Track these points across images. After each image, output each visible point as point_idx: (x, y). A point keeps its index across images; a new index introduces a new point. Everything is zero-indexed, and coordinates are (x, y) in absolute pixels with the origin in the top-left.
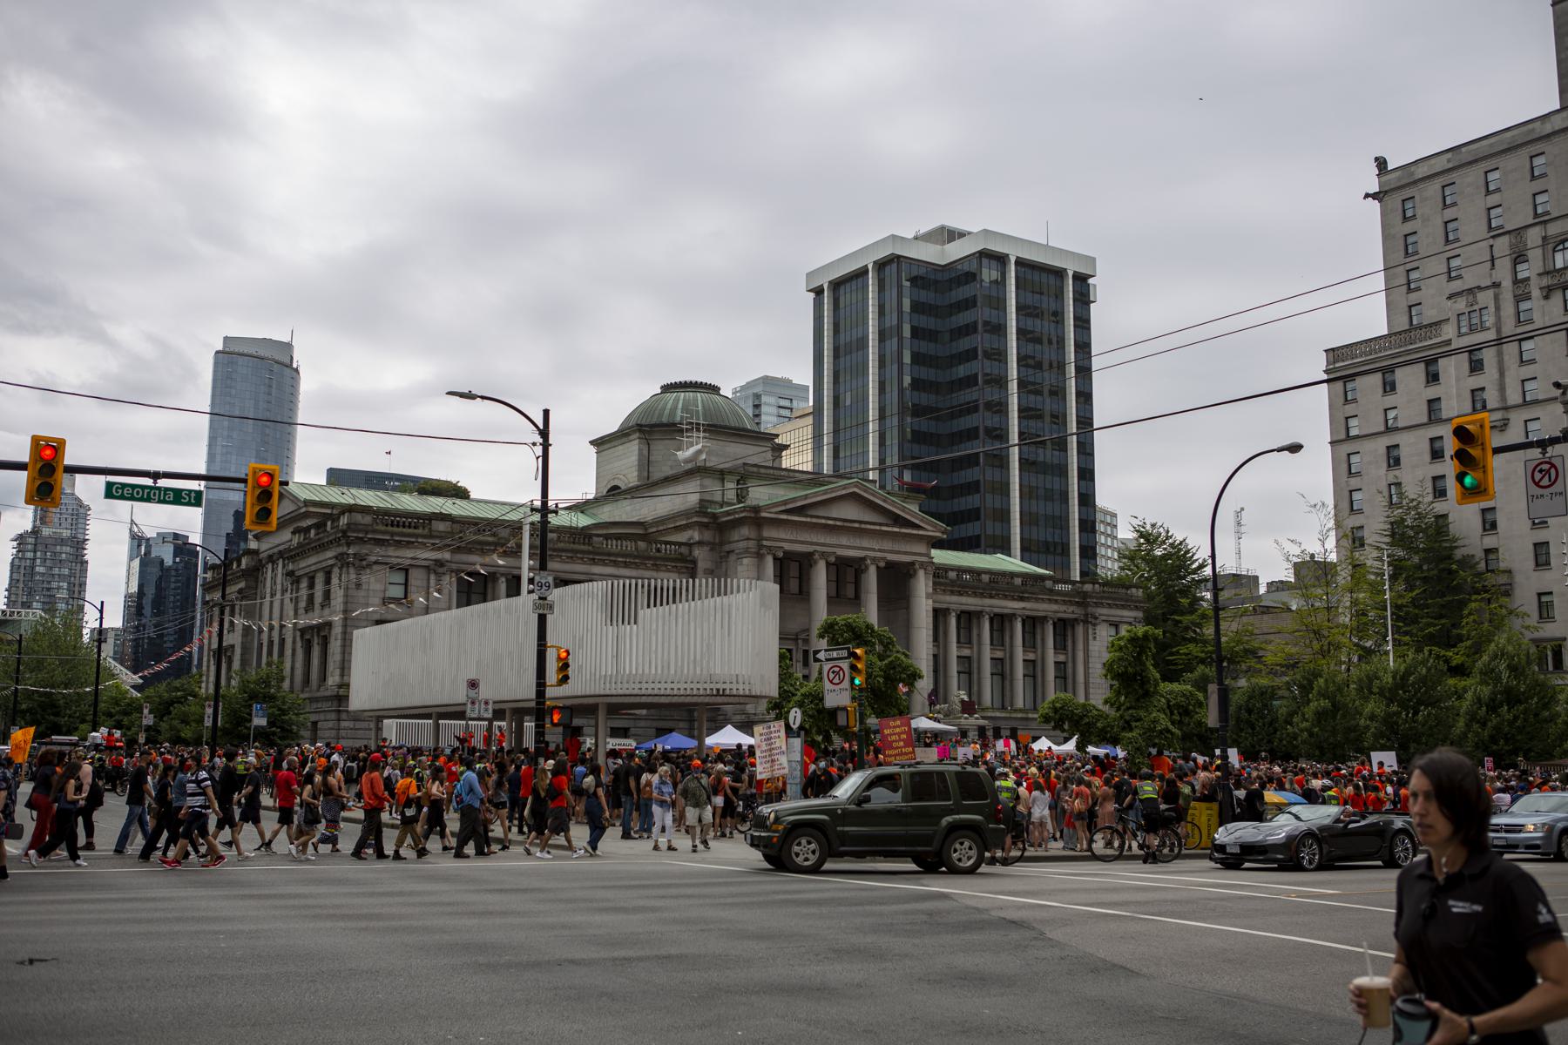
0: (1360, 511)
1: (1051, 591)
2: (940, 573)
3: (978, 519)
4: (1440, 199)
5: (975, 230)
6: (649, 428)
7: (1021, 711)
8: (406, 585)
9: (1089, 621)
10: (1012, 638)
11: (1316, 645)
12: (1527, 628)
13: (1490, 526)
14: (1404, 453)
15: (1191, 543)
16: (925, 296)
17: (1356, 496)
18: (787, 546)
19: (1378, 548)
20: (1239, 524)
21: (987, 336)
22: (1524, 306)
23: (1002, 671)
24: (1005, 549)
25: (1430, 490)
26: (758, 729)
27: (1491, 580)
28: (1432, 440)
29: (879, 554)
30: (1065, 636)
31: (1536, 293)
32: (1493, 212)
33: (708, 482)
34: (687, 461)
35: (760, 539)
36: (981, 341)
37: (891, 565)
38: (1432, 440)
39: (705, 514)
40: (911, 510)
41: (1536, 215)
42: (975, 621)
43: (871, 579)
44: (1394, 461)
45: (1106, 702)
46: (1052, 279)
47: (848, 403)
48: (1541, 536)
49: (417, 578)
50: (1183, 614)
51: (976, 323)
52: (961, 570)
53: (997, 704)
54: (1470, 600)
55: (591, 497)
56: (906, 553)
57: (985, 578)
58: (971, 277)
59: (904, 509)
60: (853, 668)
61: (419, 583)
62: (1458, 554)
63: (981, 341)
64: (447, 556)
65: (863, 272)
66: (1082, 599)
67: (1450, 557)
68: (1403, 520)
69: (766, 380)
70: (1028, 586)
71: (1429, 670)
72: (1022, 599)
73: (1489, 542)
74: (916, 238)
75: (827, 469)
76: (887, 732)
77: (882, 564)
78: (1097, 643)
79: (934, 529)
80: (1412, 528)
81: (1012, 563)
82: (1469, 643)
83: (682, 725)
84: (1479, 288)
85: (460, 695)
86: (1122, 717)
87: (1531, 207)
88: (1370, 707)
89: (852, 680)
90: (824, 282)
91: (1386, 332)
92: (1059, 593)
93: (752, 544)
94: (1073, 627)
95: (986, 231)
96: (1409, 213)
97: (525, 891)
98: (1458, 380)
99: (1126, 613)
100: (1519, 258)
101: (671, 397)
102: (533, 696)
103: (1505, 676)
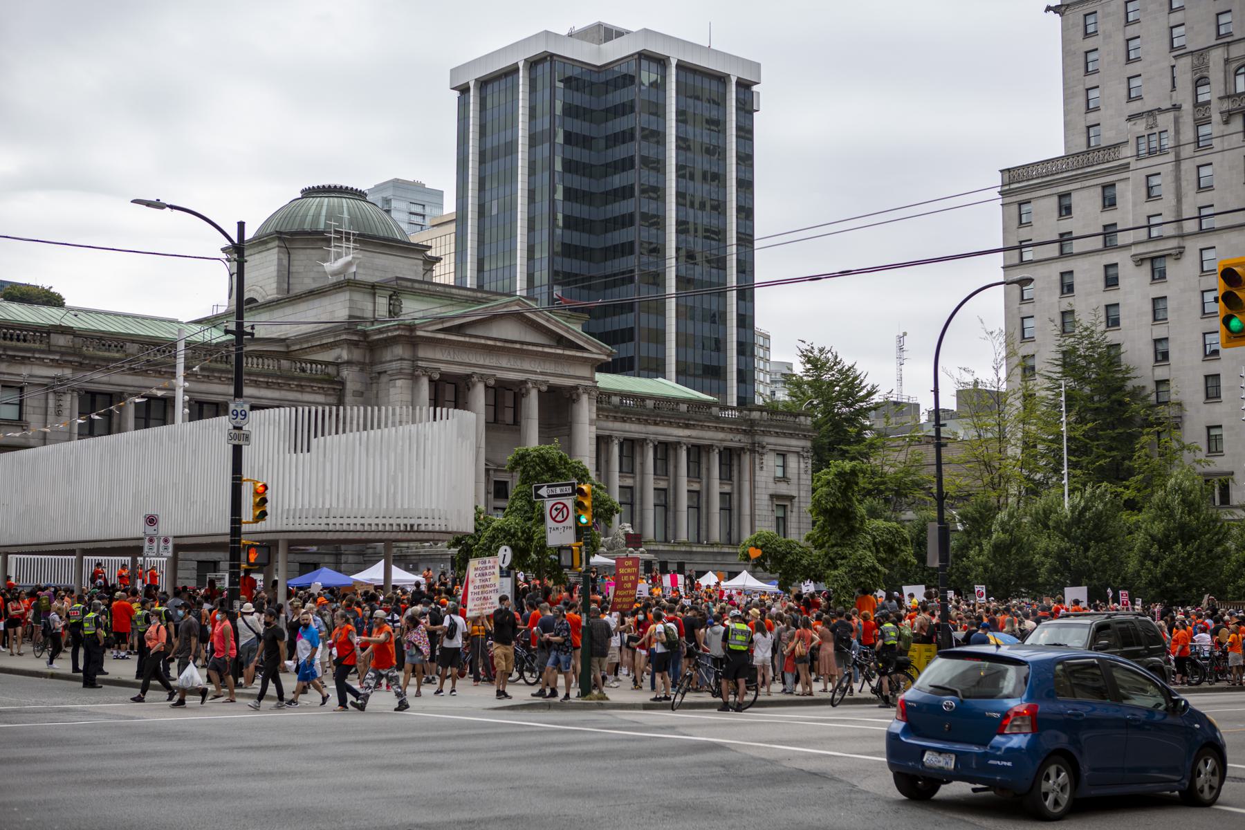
0: (1032, 339)
1: (718, 418)
2: (603, 397)
3: (632, 339)
4: (1122, 15)
5: (634, 29)
6: (291, 236)
7: (684, 544)
8: (21, 404)
9: (756, 450)
10: (676, 467)
11: (987, 479)
12: (1199, 462)
13: (1162, 357)
14: (1078, 280)
15: (859, 369)
16: (579, 99)
17: (1028, 323)
18: (444, 368)
19: (1049, 378)
20: (901, 349)
21: (644, 143)
22: (1204, 130)
23: (698, 501)
24: (656, 369)
25: (1103, 318)
26: (423, 568)
27: (1164, 412)
28: (1106, 267)
29: (540, 378)
30: (731, 466)
31: (1216, 117)
32: (1176, 32)
33: (357, 297)
34: (334, 274)
35: (415, 359)
36: (637, 149)
37: (553, 389)
38: (1106, 267)
39: (356, 332)
40: (574, 330)
41: (1219, 36)
42: (638, 449)
43: (532, 404)
44: (1067, 288)
45: (808, 539)
46: (714, 83)
47: (494, 212)
48: (1212, 367)
49: (33, 400)
50: (850, 443)
51: (633, 129)
52: (624, 395)
53: (660, 537)
54: (1141, 434)
55: (222, 310)
56: (461, 364)
57: (650, 404)
58: (628, 80)
59: (568, 330)
60: (579, 505)
61: (35, 403)
62: (1130, 385)
63: (637, 149)
64: (68, 372)
65: (512, 71)
66: (750, 428)
67: (1121, 388)
68: (1075, 349)
69: (397, 184)
70: (694, 413)
71: (1106, 504)
72: (687, 426)
73: (1161, 373)
74: (570, 35)
75: (470, 282)
76: (622, 571)
77: (544, 388)
78: (764, 473)
79: (599, 351)
80: (1085, 357)
81: (667, 386)
82: (1140, 477)
83: (327, 559)
84: (1159, 110)
85: (135, 529)
86: (826, 555)
87: (1213, 28)
88: (1043, 543)
89: (578, 519)
90: (471, 78)
91: (1063, 154)
92: (725, 421)
93: (406, 364)
94: (739, 456)
95: (646, 30)
96: (1091, 29)
97: (251, 748)
98: (1135, 205)
99: (794, 442)
100: (1200, 81)
101: (314, 202)
102: (228, 530)
103: (1178, 512)
